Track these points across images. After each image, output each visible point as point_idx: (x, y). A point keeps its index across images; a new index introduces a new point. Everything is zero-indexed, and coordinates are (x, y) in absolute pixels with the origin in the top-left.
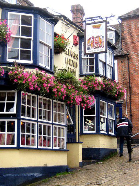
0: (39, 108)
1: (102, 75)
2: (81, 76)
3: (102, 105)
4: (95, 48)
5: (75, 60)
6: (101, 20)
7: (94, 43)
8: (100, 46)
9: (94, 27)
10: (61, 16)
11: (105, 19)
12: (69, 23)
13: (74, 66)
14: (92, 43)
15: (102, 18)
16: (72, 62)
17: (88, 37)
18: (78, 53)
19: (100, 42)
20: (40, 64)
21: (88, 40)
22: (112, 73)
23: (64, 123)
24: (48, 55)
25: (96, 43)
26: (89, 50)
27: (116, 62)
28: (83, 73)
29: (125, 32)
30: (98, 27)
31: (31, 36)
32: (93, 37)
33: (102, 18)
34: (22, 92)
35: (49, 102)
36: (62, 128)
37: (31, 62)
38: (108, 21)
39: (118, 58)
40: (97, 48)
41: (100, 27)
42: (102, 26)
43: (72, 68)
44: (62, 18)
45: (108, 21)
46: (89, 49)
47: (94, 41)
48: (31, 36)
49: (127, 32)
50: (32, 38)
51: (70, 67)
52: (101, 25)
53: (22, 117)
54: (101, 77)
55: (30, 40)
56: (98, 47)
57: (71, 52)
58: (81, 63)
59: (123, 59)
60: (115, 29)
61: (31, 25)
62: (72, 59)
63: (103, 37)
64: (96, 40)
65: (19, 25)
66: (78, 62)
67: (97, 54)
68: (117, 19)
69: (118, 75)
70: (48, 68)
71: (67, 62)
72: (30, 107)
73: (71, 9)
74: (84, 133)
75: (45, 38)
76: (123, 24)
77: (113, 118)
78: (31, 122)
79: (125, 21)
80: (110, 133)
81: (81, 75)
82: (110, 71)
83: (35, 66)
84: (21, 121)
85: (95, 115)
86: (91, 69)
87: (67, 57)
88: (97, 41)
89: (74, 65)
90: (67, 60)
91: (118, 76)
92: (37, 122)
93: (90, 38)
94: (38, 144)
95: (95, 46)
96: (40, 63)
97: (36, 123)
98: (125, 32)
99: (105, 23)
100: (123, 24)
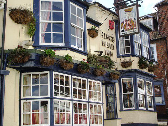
0: (73, 88)
1: (139, 55)
2: (118, 56)
3: (140, 83)
4: (128, 30)
5: (111, 43)
6: (132, 4)
7: (127, 25)
8: (133, 28)
9: (126, 11)
10: (96, 3)
11: (136, 3)
12: (104, 9)
13: (111, 48)
14: (125, 26)
15: (133, 2)
16: (108, 45)
17: (121, 21)
18: (114, 36)
19: (133, 24)
20: (72, 46)
21: (122, 23)
22: (148, 53)
23: (101, 101)
24: (81, 38)
25: (129, 25)
26: (123, 32)
27: (154, 46)
28: (120, 54)
29: (161, 18)
30: (130, 10)
31: (62, 20)
32: (126, 20)
33: (133, 2)
34: (54, 73)
35: (67, 78)
36: (99, 106)
37: (62, 44)
38: (139, 4)
39: (157, 41)
40: (130, 29)
41: (131, 10)
42: (133, 10)
43: (109, 50)
44: (97, 5)
45: (139, 4)
46: (123, 31)
47: (127, 23)
48: (62, 20)
49: (164, 18)
50: (63, 22)
51: (107, 49)
52: (132, 8)
53: (54, 96)
54: (137, 57)
55: (62, 24)
56: (131, 29)
57: (107, 35)
58: (118, 46)
59: (162, 42)
60: (153, 17)
61: (62, 10)
62: (108, 42)
63: (135, 19)
64: (129, 22)
65: (50, 11)
66: (115, 44)
67: (131, 35)
68: (154, 7)
69: (157, 57)
70: (82, 49)
71: (104, 44)
72: (81, 90)
73: (114, 2)
74: (21, 101)
75: (77, 23)
76: (160, 11)
77: (152, 95)
78: (83, 103)
79: (161, 8)
80: (149, 109)
81: (119, 56)
82: (146, 52)
83: (67, 47)
84: (54, 100)
85: (133, 93)
86: (128, 50)
87: (103, 40)
88: (130, 23)
89: (111, 47)
90: (103, 43)
91: (158, 58)
92: (88, 102)
93: (124, 21)
94: (73, 122)
95: (129, 28)
96: (72, 45)
97: (87, 104)
98: (161, 18)
99: (136, 6)
100: (160, 11)
